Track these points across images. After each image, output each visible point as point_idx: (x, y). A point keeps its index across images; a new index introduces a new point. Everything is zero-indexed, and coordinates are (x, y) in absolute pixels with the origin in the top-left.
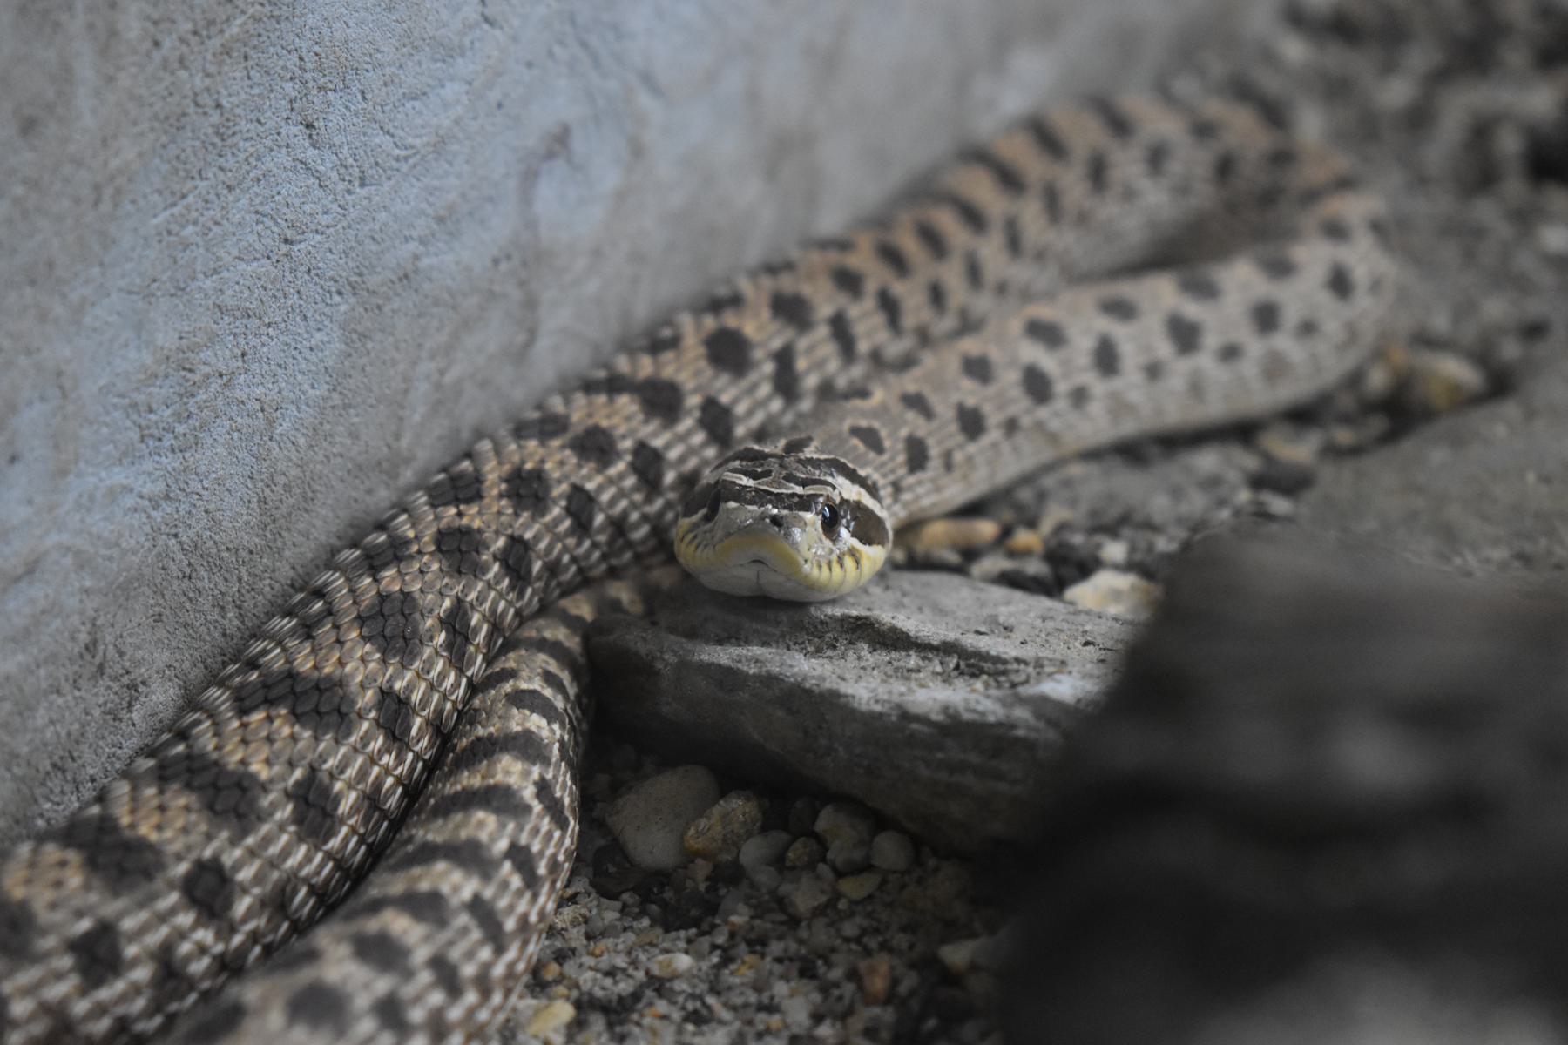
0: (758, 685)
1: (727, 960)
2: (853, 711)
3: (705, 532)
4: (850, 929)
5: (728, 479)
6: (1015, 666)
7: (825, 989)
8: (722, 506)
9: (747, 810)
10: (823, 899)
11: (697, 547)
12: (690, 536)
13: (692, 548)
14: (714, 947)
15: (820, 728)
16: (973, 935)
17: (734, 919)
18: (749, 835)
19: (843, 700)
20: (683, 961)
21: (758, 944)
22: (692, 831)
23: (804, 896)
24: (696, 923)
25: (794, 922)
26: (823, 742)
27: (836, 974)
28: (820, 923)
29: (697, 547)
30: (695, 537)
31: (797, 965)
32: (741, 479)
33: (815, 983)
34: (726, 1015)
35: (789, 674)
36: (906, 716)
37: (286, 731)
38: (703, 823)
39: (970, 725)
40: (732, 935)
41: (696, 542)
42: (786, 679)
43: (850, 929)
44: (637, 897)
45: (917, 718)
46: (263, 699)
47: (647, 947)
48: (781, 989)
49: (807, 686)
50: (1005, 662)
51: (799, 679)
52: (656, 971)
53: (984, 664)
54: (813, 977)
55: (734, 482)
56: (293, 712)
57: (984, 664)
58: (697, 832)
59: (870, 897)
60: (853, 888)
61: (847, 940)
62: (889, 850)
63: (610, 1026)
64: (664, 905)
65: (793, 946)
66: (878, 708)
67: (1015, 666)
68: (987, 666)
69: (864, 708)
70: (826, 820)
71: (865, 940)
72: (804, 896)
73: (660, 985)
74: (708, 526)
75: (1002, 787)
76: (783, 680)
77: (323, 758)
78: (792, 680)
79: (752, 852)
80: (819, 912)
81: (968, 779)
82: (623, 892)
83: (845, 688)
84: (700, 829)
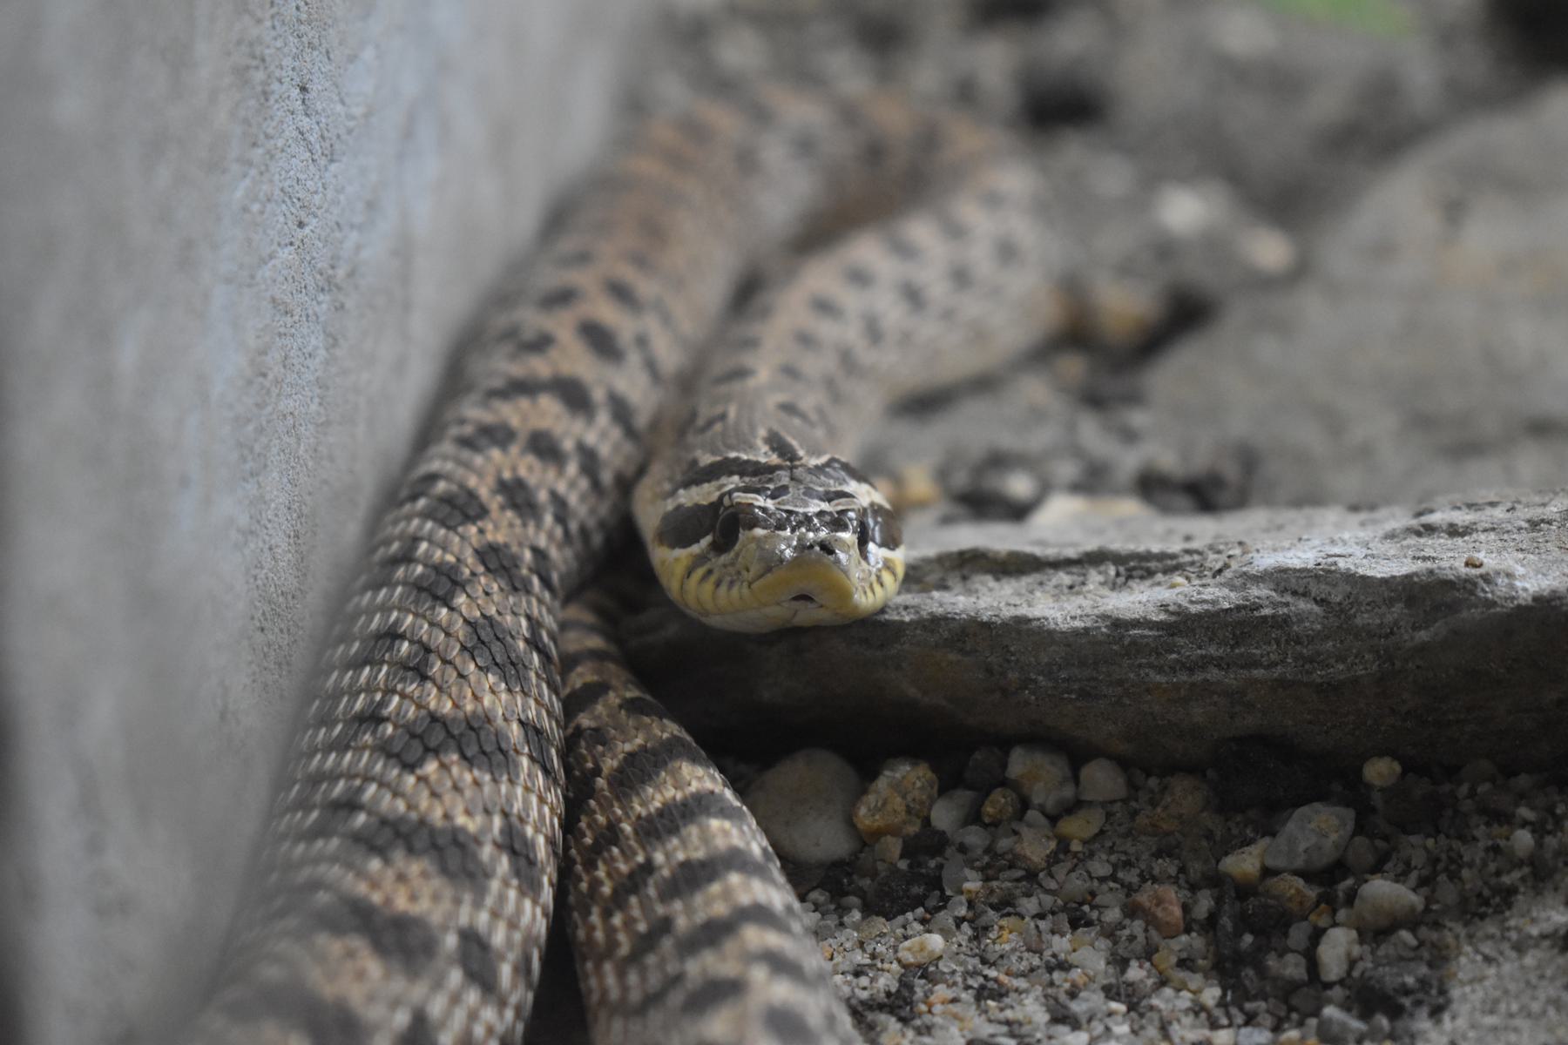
0: (918, 632)
1: (980, 932)
2: (1051, 633)
3: (725, 566)
4: (1100, 868)
5: (743, 501)
6: (1187, 558)
7: (1110, 933)
8: (743, 535)
9: (921, 774)
10: (1053, 845)
11: (718, 584)
12: (700, 572)
13: (708, 586)
14: (959, 921)
15: (1009, 661)
16: (1249, 842)
17: (968, 886)
18: (932, 802)
19: (1035, 624)
20: (936, 941)
21: (1005, 905)
22: (863, 811)
23: (1034, 846)
24: (918, 901)
25: (1031, 876)
26: (1013, 676)
27: (1113, 915)
28: (1060, 871)
29: (718, 584)
30: (710, 572)
31: (1063, 919)
32: (757, 500)
33: (1093, 932)
34: (1021, 983)
35: (958, 611)
36: (1118, 624)
37: (468, 777)
38: (871, 799)
39: (1199, 617)
40: (971, 905)
41: (713, 579)
42: (957, 617)
43: (1100, 868)
44: (827, 894)
45: (1136, 623)
46: (1047, 314)
47: (878, 939)
48: (1061, 944)
49: (985, 619)
50: (1173, 556)
51: (972, 614)
52: (910, 958)
53: (1149, 565)
54: (1089, 924)
55: (752, 504)
56: (463, 756)
57: (1149, 565)
58: (869, 810)
59: (1102, 832)
60: (1078, 827)
61: (1102, 880)
62: (1102, 779)
63: (904, 1021)
64: (861, 893)
65: (1048, 900)
66: (1078, 624)
67: (1187, 558)
68: (1153, 565)
69: (1064, 627)
70: (1019, 763)
71: (1120, 875)
72: (1034, 846)
73: (926, 971)
74: (724, 558)
75: (1258, 673)
76: (954, 619)
77: (510, 799)
78: (964, 616)
79: (944, 816)
80: (1053, 859)
81: (1214, 674)
82: (809, 891)
83: (1024, 611)
84: (872, 806)
